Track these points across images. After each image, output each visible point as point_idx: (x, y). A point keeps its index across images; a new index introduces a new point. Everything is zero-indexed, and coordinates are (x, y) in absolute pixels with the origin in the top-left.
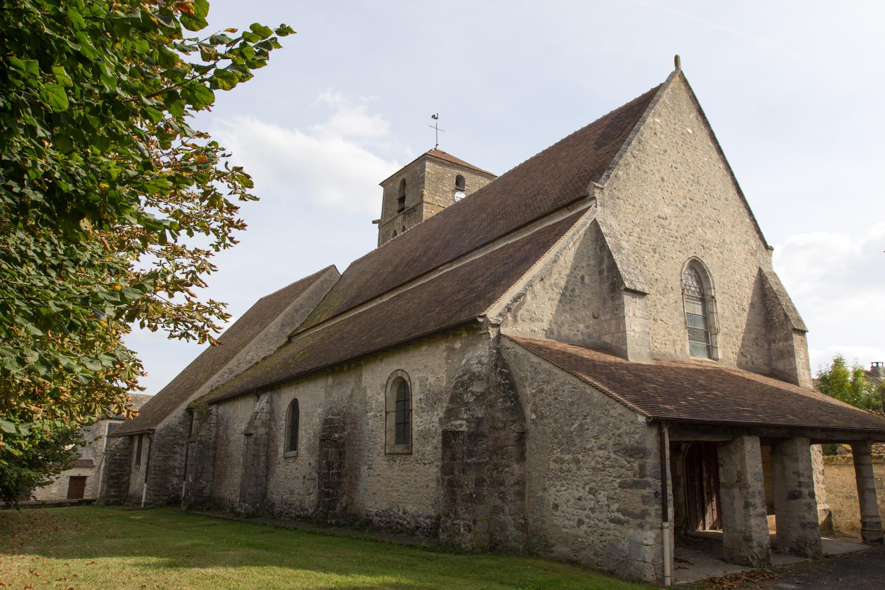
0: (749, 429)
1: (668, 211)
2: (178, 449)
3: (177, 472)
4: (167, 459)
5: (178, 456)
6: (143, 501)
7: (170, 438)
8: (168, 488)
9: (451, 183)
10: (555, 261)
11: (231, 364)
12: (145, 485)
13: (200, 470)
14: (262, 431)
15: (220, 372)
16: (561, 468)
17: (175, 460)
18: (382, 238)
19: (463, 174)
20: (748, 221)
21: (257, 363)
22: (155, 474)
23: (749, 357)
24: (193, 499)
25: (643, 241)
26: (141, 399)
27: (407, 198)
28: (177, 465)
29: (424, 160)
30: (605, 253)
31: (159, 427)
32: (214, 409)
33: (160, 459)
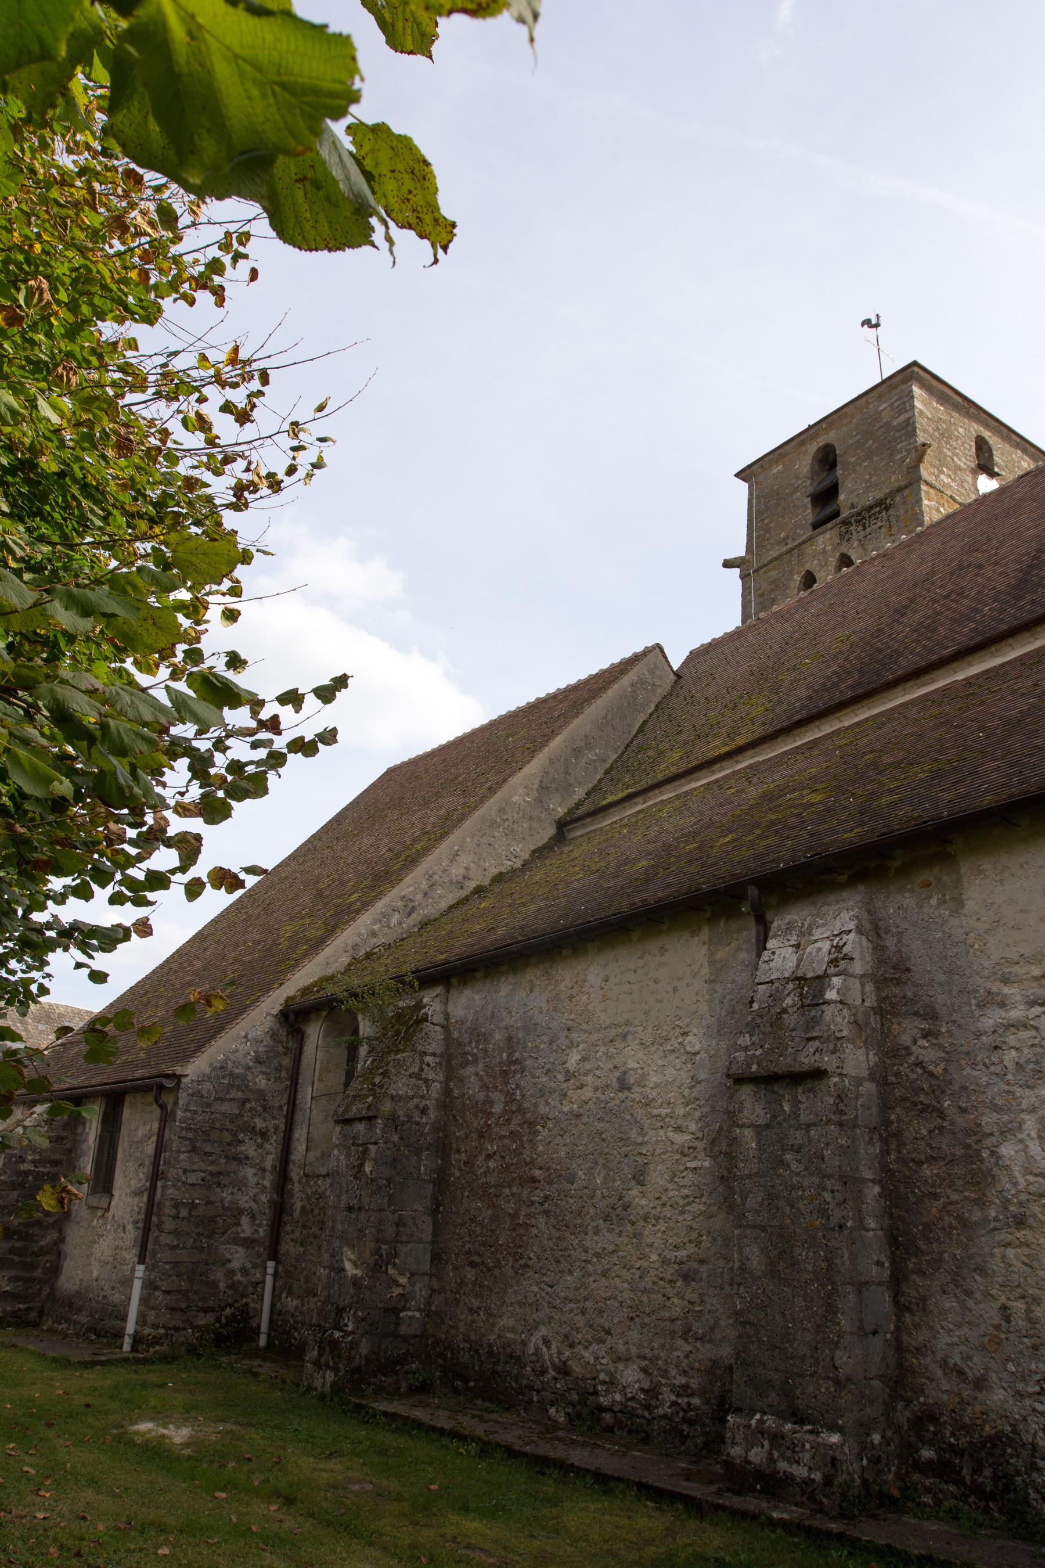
2: (249, 1148)
3: (246, 1228)
4: (214, 1180)
5: (249, 1172)
6: (130, 1327)
7: (225, 1107)
8: (214, 1284)
9: (967, 458)
11: (411, 884)
12: (140, 1270)
13: (390, 1232)
15: (380, 905)
17: (241, 1185)
18: (755, 599)
21: (479, 891)
22: (176, 1233)
24: (365, 1348)
28: (245, 1201)
29: (905, 381)
31: (196, 1068)
32: (431, 1000)
33: (193, 1178)
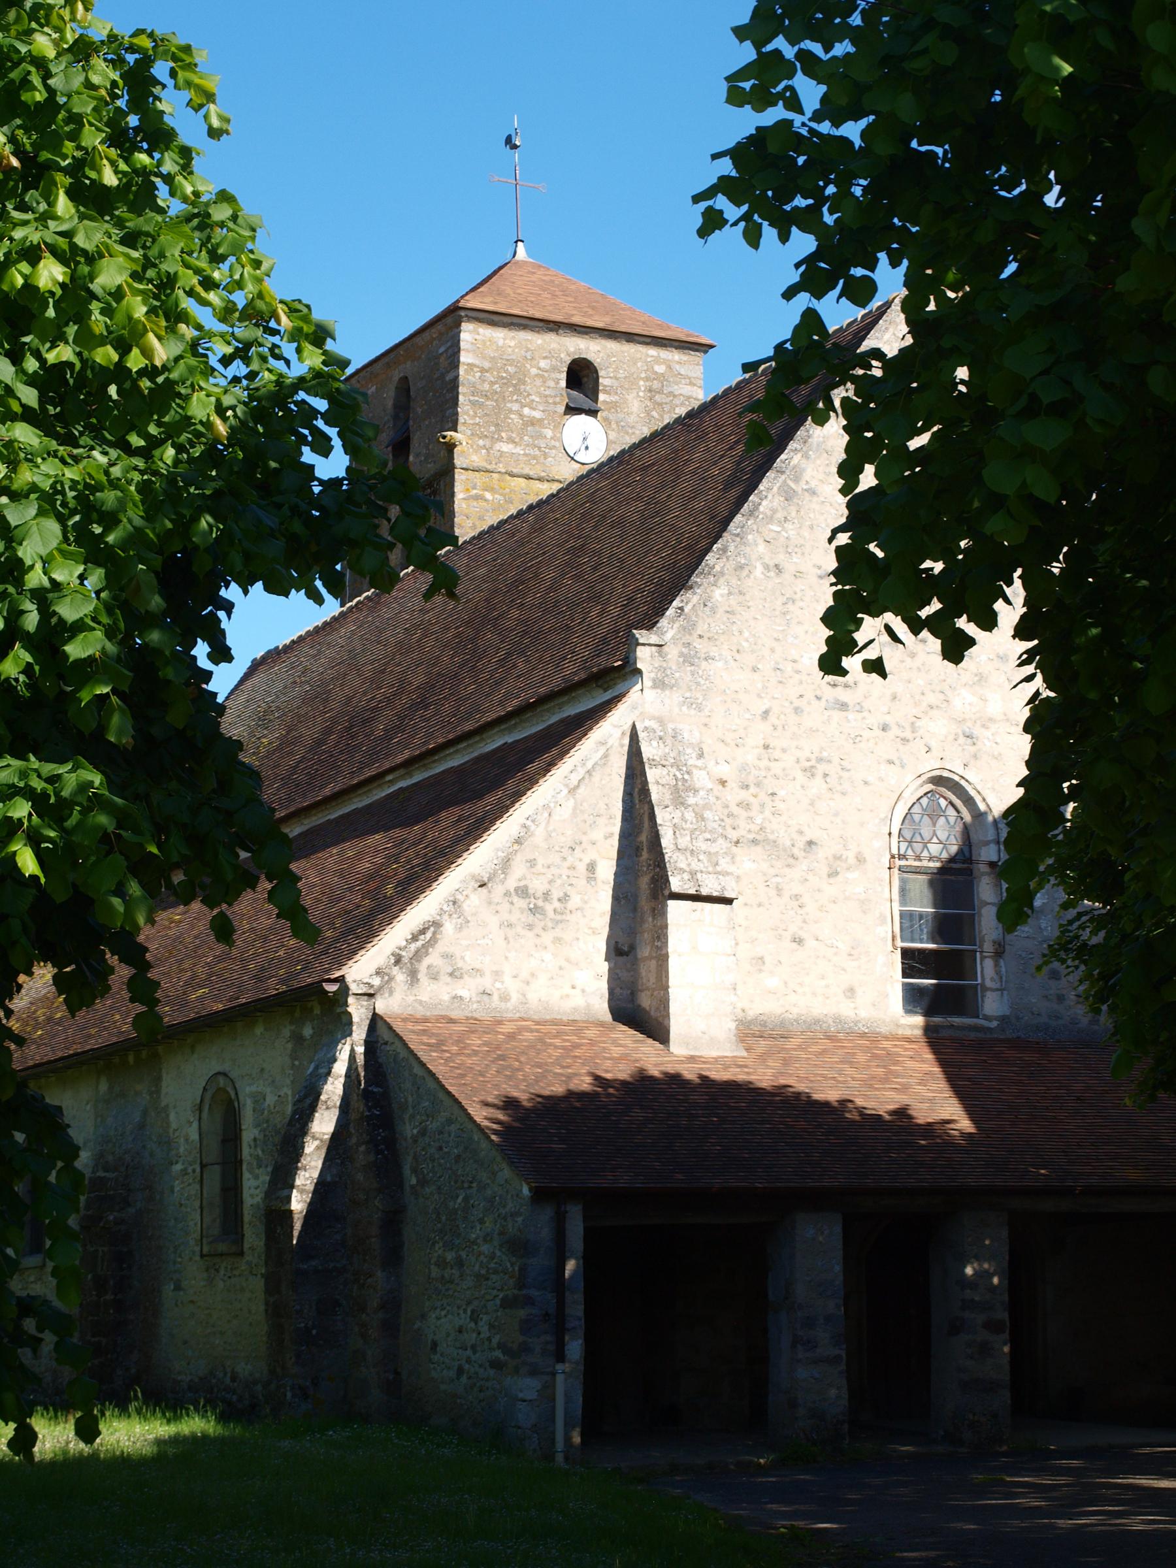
10: (518, 841)
16: (443, 1277)
19: (592, 349)
25: (777, 754)
30: (646, 807)
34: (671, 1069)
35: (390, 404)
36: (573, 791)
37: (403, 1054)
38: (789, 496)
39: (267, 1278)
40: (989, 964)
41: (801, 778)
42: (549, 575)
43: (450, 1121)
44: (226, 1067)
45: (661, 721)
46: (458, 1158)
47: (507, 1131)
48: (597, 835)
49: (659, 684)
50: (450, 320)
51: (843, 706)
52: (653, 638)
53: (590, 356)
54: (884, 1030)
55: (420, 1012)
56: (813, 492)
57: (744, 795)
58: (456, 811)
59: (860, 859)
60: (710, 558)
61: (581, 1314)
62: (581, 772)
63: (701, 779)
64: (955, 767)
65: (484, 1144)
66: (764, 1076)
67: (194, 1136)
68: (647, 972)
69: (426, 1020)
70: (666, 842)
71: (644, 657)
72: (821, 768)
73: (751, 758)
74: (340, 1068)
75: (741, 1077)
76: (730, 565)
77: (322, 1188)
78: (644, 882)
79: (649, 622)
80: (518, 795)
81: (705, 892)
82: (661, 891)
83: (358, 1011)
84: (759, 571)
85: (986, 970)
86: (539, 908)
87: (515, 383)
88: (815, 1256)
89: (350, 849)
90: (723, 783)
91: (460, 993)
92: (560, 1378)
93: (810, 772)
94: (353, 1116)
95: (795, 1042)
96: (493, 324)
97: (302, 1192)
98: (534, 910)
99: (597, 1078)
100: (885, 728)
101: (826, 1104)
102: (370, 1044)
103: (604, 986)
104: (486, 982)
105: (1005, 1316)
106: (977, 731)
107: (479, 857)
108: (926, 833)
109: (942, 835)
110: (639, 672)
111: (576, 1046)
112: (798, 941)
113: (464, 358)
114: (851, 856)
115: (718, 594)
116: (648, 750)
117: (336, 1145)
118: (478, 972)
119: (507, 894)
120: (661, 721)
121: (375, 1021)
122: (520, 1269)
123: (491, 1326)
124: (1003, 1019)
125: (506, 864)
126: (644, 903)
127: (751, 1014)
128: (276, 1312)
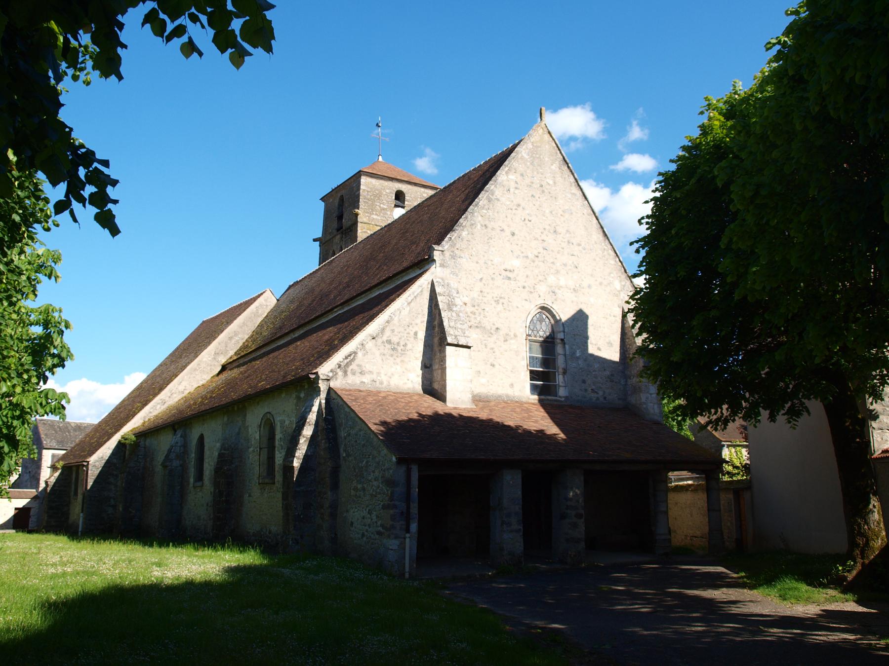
0: (511, 464)
1: (515, 263)
2: (112, 480)
10: (388, 322)
14: (176, 463)
19: (404, 187)
20: (613, 262)
23: (601, 393)
25: (485, 294)
26: (85, 427)
27: (345, 216)
34: (447, 411)
35: (337, 204)
36: (409, 304)
37: (341, 403)
38: (490, 200)
39: (283, 494)
40: (561, 377)
41: (494, 304)
42: (394, 242)
43: (360, 430)
44: (270, 410)
45: (442, 279)
46: (364, 445)
47: (384, 434)
48: (418, 321)
49: (442, 265)
50: (359, 175)
51: (509, 278)
52: (440, 248)
53: (405, 191)
54: (524, 400)
55: (348, 387)
56: (498, 200)
57: (473, 309)
58: (362, 316)
59: (515, 336)
60: (461, 220)
61: (417, 512)
62: (412, 297)
63: (458, 301)
64: (549, 303)
65: (375, 439)
66: (483, 415)
67: (258, 437)
68: (437, 375)
69: (350, 390)
70: (445, 324)
71: (437, 255)
72: (501, 301)
73: (476, 296)
74: (315, 409)
75: (475, 416)
76: (469, 223)
77: (306, 457)
78: (436, 340)
79: (439, 243)
80: (387, 306)
81: (460, 343)
82: (443, 342)
83: (323, 386)
84: (479, 226)
85: (560, 379)
86: (395, 348)
87: (378, 196)
88: (510, 487)
89: (320, 334)
90: (465, 304)
91: (364, 380)
92: (408, 540)
93: (497, 302)
94: (320, 428)
95: (493, 403)
96: (372, 177)
97: (298, 459)
98: (393, 349)
99: (420, 415)
100: (524, 287)
101: (509, 426)
102: (327, 400)
103: (420, 380)
104: (374, 377)
105: (582, 512)
106: (557, 291)
107: (372, 328)
108: (538, 327)
109: (544, 328)
110: (434, 260)
111: (410, 402)
112: (493, 365)
113: (362, 187)
114: (512, 334)
115: (464, 234)
116: (438, 289)
117: (313, 440)
118: (371, 372)
119: (383, 342)
120: (442, 279)
121: (330, 390)
122: (391, 493)
123: (377, 517)
124: (566, 397)
125: (383, 330)
126: (436, 348)
127: (475, 393)
128: (286, 508)
